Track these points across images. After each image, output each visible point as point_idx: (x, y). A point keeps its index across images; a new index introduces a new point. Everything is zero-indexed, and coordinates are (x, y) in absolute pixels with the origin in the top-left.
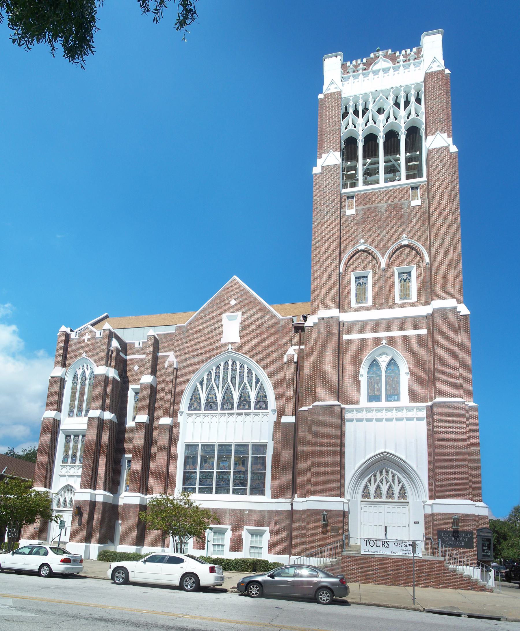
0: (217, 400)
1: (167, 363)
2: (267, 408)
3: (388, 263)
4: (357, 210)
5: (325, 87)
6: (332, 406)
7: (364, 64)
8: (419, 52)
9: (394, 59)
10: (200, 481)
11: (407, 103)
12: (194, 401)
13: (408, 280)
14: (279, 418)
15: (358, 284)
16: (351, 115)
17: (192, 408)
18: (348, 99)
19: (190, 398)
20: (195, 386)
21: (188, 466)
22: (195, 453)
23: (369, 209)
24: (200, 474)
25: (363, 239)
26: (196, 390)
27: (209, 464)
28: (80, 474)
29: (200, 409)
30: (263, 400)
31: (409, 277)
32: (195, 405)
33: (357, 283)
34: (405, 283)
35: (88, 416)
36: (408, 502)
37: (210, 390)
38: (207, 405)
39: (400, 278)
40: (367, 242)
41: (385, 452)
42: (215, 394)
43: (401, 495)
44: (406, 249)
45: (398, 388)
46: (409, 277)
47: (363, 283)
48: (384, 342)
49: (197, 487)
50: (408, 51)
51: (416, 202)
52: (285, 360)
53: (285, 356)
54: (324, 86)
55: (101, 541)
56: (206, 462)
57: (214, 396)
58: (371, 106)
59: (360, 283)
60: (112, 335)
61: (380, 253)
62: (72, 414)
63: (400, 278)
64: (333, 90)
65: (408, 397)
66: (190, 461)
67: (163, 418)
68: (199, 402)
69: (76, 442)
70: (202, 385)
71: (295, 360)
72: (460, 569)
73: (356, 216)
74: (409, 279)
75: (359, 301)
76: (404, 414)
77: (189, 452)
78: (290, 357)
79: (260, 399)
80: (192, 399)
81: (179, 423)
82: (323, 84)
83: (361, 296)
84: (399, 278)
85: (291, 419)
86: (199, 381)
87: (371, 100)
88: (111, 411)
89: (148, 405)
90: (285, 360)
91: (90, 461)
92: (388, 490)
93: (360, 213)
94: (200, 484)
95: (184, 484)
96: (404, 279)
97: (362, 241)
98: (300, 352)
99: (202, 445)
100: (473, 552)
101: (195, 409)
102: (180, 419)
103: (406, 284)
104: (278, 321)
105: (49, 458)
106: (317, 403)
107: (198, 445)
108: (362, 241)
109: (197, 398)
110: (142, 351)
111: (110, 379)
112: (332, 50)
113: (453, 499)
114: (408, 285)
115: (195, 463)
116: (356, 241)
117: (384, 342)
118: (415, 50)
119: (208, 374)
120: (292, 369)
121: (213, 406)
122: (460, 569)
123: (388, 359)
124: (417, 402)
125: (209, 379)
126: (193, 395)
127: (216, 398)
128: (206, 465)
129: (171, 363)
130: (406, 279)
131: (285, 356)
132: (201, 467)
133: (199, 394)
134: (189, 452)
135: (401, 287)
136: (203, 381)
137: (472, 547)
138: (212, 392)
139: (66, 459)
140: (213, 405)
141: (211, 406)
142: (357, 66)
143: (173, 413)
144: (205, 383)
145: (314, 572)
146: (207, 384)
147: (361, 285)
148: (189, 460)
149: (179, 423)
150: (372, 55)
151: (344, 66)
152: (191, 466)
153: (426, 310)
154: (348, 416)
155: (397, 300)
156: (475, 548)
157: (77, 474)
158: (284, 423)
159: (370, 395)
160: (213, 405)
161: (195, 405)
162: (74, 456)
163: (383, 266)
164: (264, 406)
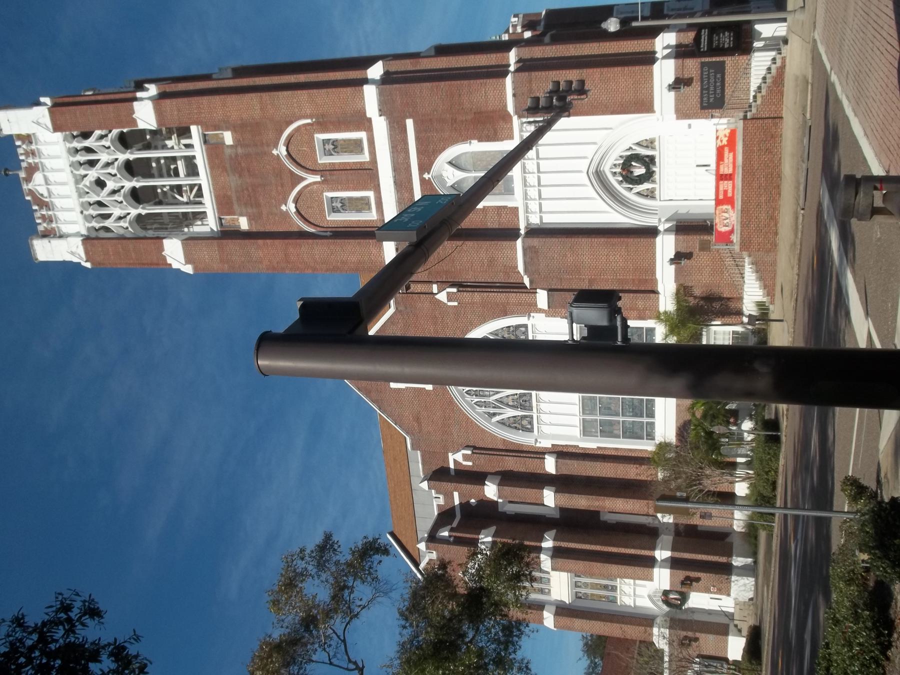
0: (517, 394)
1: (465, 463)
2: (526, 326)
3: (313, 171)
4: (242, 215)
5: (75, 260)
6: (525, 250)
7: (41, 208)
8: (19, 137)
9: (32, 170)
10: (636, 415)
11: (89, 150)
12: (519, 424)
13: (335, 143)
14: (541, 311)
15: (343, 209)
16: (108, 223)
17: (529, 427)
18: (89, 229)
19: (514, 431)
20: (497, 423)
21: (616, 432)
22: (595, 423)
23: (238, 199)
24: (626, 416)
25: (280, 205)
26: (502, 423)
27: (610, 404)
28: (632, 581)
29: (532, 417)
30: (513, 331)
31: (331, 142)
32: (525, 422)
33: (342, 211)
34: (339, 147)
35: (549, 570)
36: (659, 137)
37: (502, 402)
38: (523, 408)
39: (333, 153)
40: (276, 146)
41: (588, 173)
42: (507, 396)
43: (650, 145)
44: (291, 148)
45: (492, 153)
46: (331, 142)
47: (341, 203)
48: (426, 176)
49: (645, 420)
50: (20, 151)
51: (228, 138)
52: (456, 304)
53: (450, 304)
54: (67, 260)
55: (729, 552)
56: (609, 409)
57: (511, 398)
58: (94, 198)
59: (342, 206)
60: (432, 538)
61: (299, 183)
62: (547, 591)
63: (333, 153)
64: (81, 251)
65: (505, 141)
66: (607, 428)
67: (546, 467)
68: (519, 418)
69: (586, 585)
70: (494, 414)
71: (454, 290)
72: (755, 82)
73: (250, 216)
74: (334, 142)
75: (367, 206)
76: (532, 179)
77: (594, 430)
78: (450, 297)
79: (513, 335)
80: (516, 428)
81: (553, 445)
82: (71, 262)
83: (362, 205)
84: (332, 155)
85: (542, 298)
86: (489, 418)
87: (86, 199)
88: (541, 539)
89: (528, 490)
90: (456, 304)
91: (614, 568)
92: (643, 195)
93: (244, 211)
94: (642, 416)
95: (641, 438)
96: (334, 149)
97: (284, 208)
98: (443, 285)
99: (583, 413)
100: (729, 61)
101: (531, 423)
102: (546, 444)
103: (341, 145)
104: (202, 127)
105: (611, 621)
106: (521, 268)
107: (583, 419)
108: (284, 208)
109: (514, 420)
110: (449, 496)
111: (652, 552)
112: (28, 252)
113: (652, 87)
114: (342, 142)
115: (611, 423)
116: (286, 214)
117: (426, 176)
118: (18, 143)
119: (478, 406)
120: (467, 296)
121: (524, 398)
122: (755, 82)
123: (451, 169)
124: (511, 129)
125: (486, 405)
126: (509, 426)
127: (514, 395)
128: (612, 408)
129: (466, 457)
130: (333, 145)
131: (450, 304)
132: (617, 415)
133: (509, 418)
134: (594, 430)
135: (346, 152)
136: (489, 413)
137: (724, 62)
138: (505, 400)
139: (611, 598)
140: (523, 399)
141: (526, 401)
142: (43, 217)
143: (540, 454)
144: (492, 411)
145: (838, 101)
146: (494, 407)
147: (343, 205)
148: (607, 430)
149: (553, 445)
150: (28, 198)
151: (46, 235)
152: (615, 427)
153: (380, 125)
154: (535, 220)
155: (366, 157)
156: (725, 58)
157: (632, 584)
158: (549, 303)
159: (503, 191)
160: (523, 399)
161: (525, 422)
162: (606, 587)
163: (317, 178)
164: (523, 329)
